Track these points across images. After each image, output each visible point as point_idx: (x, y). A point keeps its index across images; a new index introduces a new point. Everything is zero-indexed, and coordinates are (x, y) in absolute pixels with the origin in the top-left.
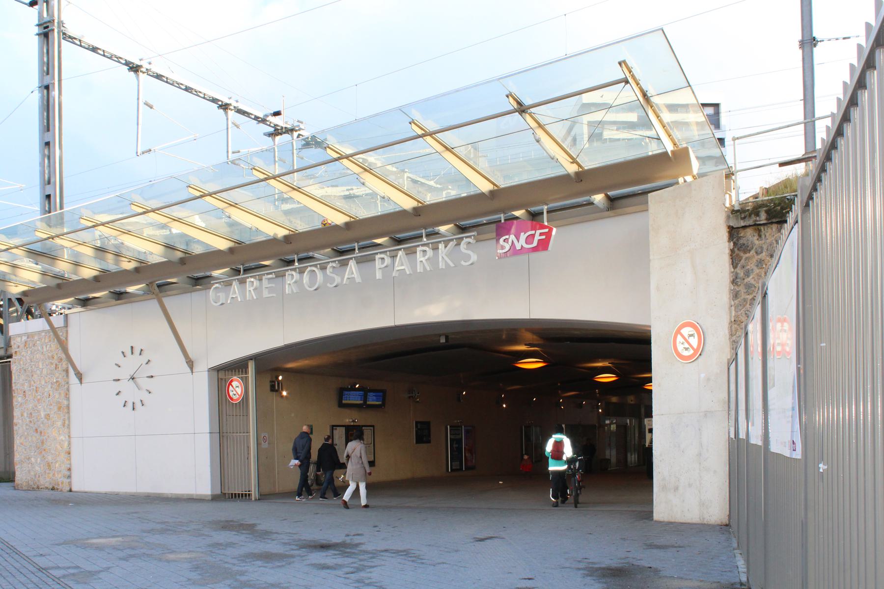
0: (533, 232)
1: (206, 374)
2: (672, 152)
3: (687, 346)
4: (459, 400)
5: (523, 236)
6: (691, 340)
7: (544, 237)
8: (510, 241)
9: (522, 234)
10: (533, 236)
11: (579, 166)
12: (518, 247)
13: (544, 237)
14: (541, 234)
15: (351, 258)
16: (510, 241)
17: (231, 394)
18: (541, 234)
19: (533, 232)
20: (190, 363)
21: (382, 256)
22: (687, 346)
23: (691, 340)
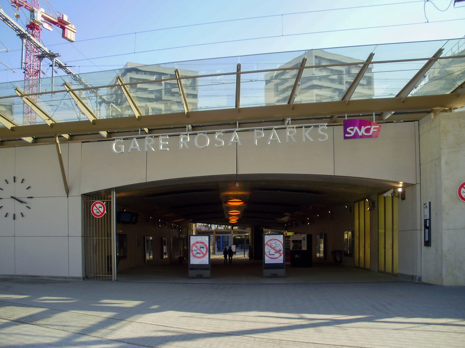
0: (370, 127)
1: (80, 198)
2: (138, 117)
3: (98, 211)
4: (325, 235)
5: (363, 129)
6: (100, 209)
7: (376, 130)
8: (355, 131)
9: (363, 127)
10: (370, 129)
11: (53, 121)
12: (360, 134)
13: (376, 130)
14: (374, 128)
15: (134, 137)
16: (355, 131)
17: (95, 212)
18: (374, 128)
19: (370, 127)
20: (68, 191)
21: (185, 136)
22: (98, 211)
23: (100, 209)
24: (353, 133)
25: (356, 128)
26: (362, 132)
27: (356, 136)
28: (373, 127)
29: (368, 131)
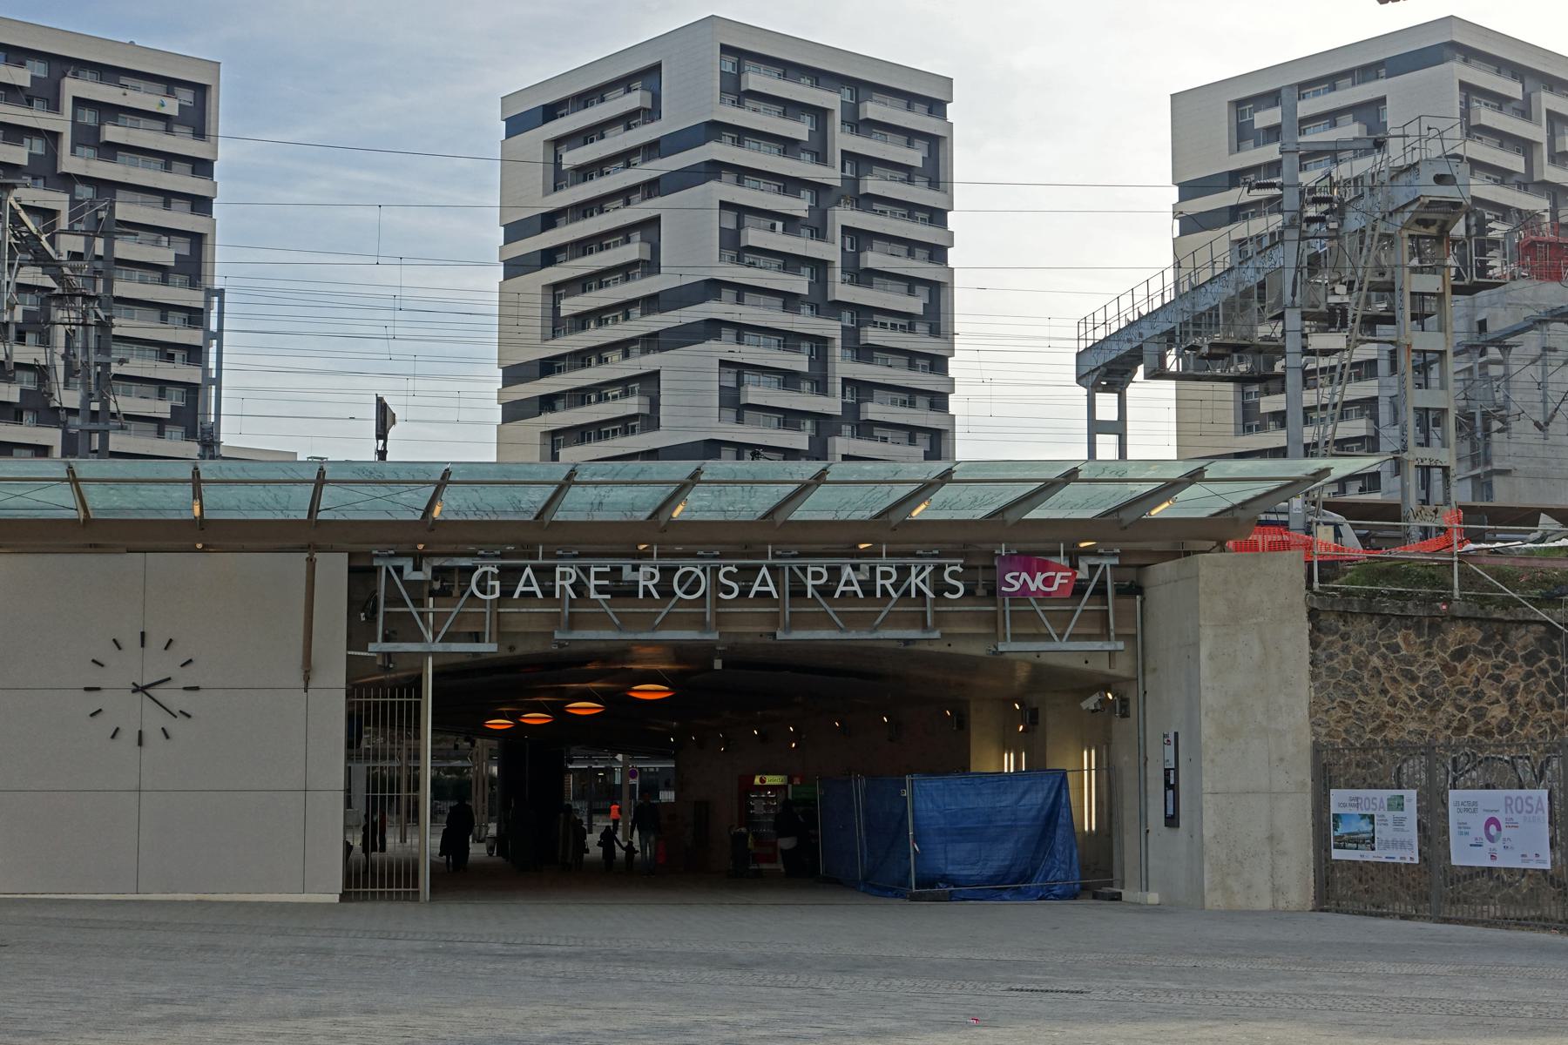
5: (1040, 577)
10: (1053, 578)
12: (1033, 588)
24: (1017, 586)
25: (1024, 575)
28: (1060, 575)
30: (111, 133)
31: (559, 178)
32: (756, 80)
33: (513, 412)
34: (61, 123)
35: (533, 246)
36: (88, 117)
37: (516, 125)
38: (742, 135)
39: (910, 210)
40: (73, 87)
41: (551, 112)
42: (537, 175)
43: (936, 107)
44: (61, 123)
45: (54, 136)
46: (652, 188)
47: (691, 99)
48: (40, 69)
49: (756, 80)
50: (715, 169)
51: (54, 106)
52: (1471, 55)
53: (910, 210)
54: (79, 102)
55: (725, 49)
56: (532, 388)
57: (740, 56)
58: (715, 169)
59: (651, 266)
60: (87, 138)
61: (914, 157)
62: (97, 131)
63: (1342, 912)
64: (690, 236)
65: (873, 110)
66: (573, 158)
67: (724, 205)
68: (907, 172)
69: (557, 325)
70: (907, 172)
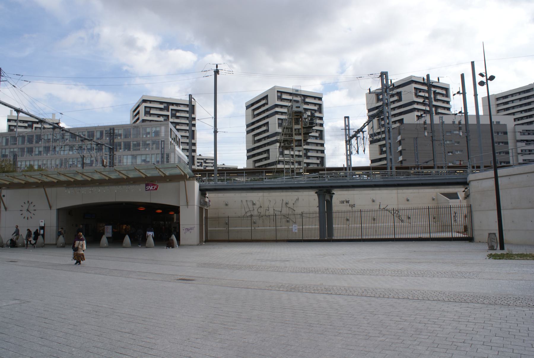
1: (56, 211)
20: (50, 207)
26: (151, 188)
27: (149, 190)
29: (153, 188)
30: (178, 114)
31: (255, 116)
32: (284, 96)
33: (249, 157)
34: (169, 113)
35: (251, 128)
36: (174, 112)
37: (248, 107)
38: (282, 106)
39: (444, 102)
40: (171, 107)
41: (252, 105)
42: (251, 117)
43: (320, 99)
44: (169, 113)
45: (168, 116)
46: (267, 117)
47: (273, 100)
48: (166, 105)
49: (284, 96)
50: (277, 113)
51: (168, 111)
52: (416, 82)
53: (444, 102)
54: (172, 110)
55: (278, 91)
56: (251, 153)
57: (281, 93)
58: (277, 113)
59: (267, 131)
60: (174, 116)
61: (444, 92)
62: (176, 114)
63: (509, 256)
64: (274, 125)
65: (308, 100)
66: (256, 112)
67: (279, 119)
68: (442, 95)
69: (255, 142)
70: (442, 95)
